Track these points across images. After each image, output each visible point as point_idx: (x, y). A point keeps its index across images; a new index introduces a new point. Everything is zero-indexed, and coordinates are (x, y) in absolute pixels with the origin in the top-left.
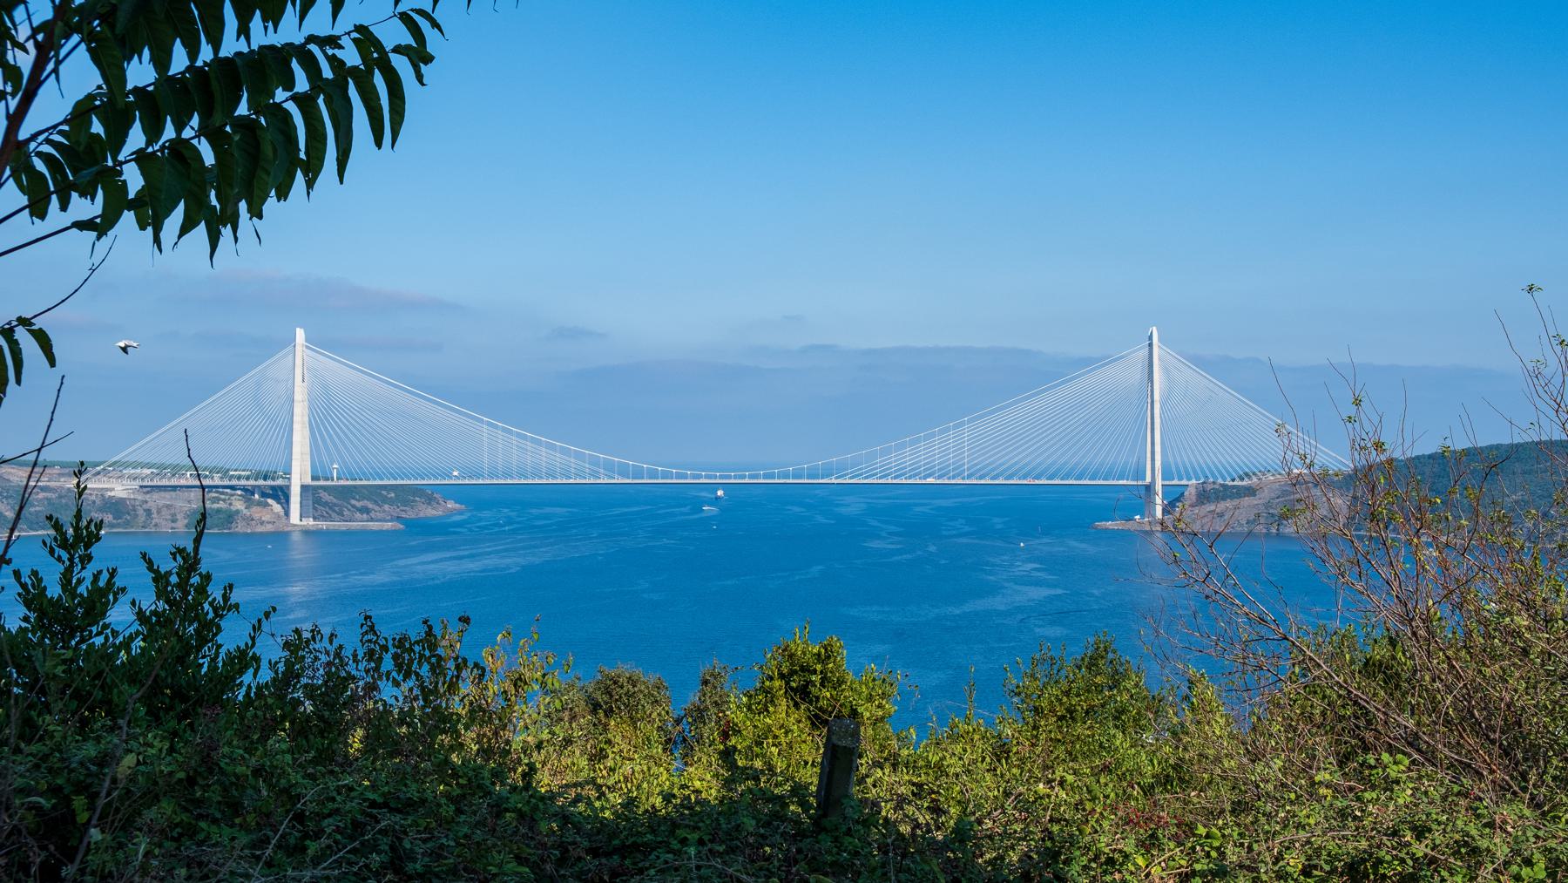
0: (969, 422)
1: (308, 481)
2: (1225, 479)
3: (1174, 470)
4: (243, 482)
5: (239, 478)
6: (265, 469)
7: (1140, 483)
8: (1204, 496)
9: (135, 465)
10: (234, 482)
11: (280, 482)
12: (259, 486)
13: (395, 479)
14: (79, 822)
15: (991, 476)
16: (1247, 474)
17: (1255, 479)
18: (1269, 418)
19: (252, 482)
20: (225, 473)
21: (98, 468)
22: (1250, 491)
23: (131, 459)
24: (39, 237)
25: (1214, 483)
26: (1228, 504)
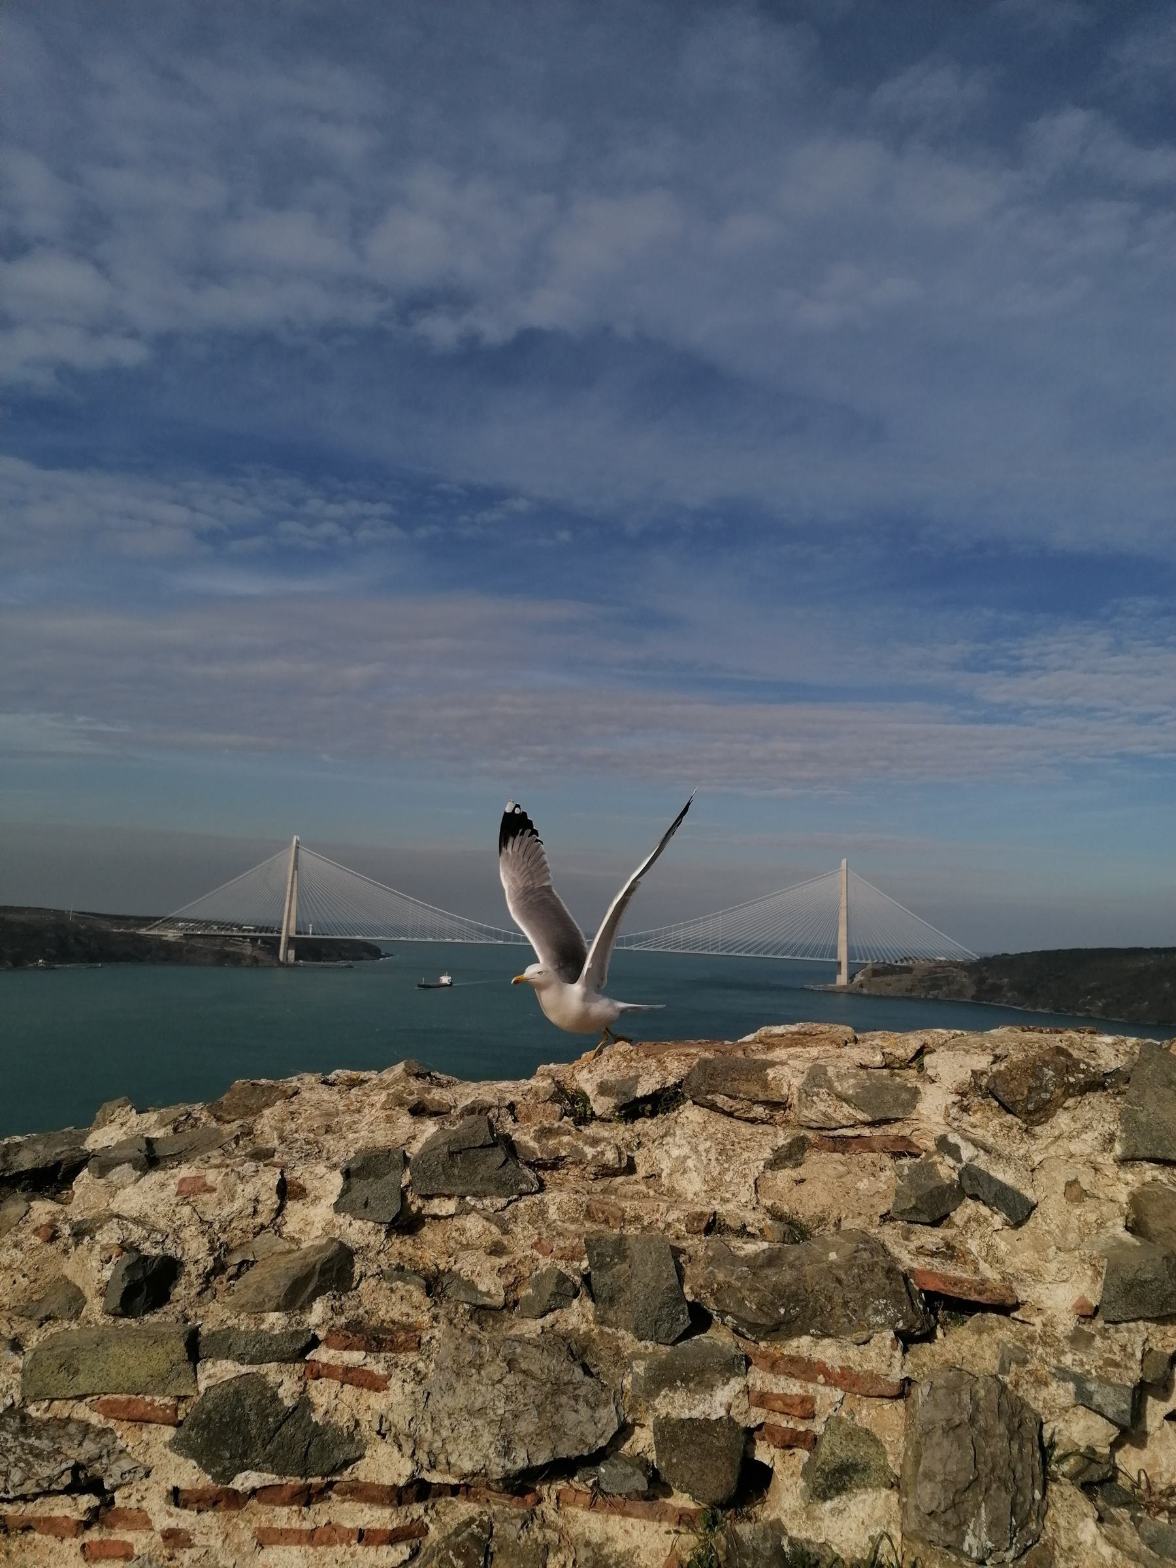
0: (723, 914)
1: (293, 934)
2: (890, 961)
3: (857, 952)
4: (252, 934)
5: (249, 931)
6: (266, 925)
7: (833, 960)
8: (876, 973)
9: (184, 920)
10: (246, 934)
11: (275, 935)
12: (261, 937)
13: (350, 935)
14: (646, 1488)
15: (773, 951)
16: (906, 959)
17: (911, 962)
18: (370, 882)
19: (257, 934)
20: (240, 928)
21: (157, 922)
22: (908, 970)
23: (186, 916)
24: (673, 838)
25: (884, 963)
26: (894, 978)
